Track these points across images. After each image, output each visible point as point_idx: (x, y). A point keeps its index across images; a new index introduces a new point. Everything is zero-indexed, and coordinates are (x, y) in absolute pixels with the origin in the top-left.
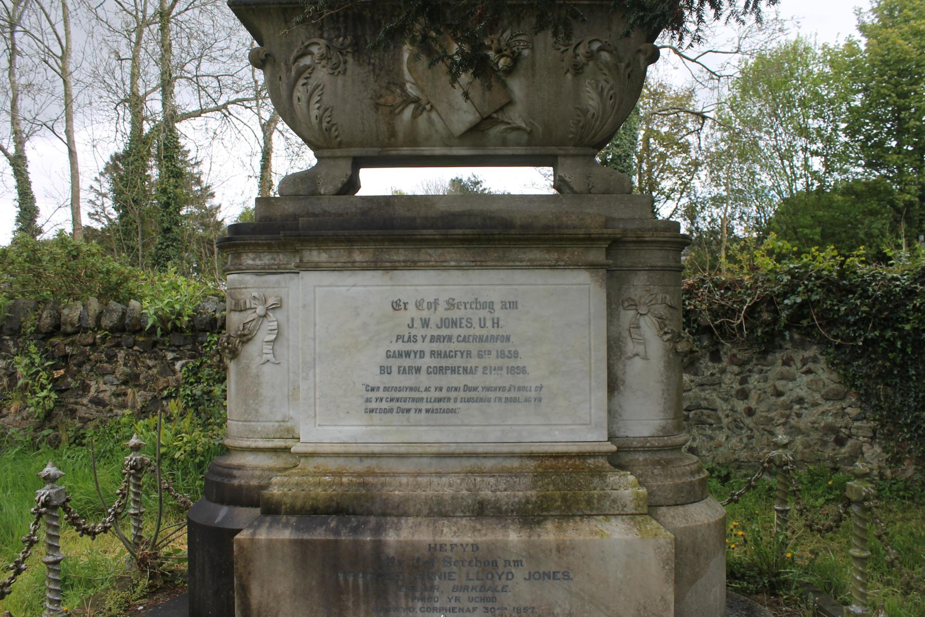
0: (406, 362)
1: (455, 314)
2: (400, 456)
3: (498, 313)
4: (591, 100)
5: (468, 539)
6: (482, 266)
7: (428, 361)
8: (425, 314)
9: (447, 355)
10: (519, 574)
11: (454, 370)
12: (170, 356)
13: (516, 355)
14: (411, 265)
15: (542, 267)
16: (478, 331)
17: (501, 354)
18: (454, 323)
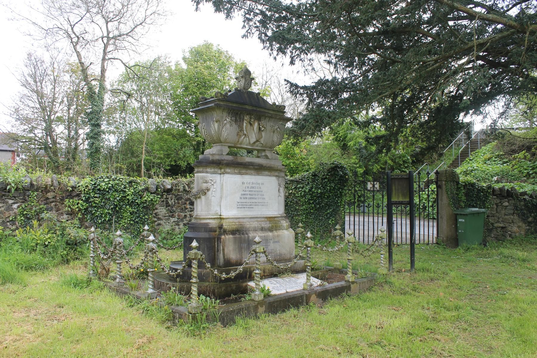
0: (245, 196)
1: (253, 185)
2: (244, 218)
3: (261, 186)
4: (275, 139)
5: (263, 235)
6: (258, 174)
7: (248, 196)
8: (248, 185)
9: (252, 195)
10: (272, 242)
11: (253, 198)
12: (11, 202)
13: (263, 195)
14: (247, 174)
15: (267, 176)
16: (257, 190)
17: (261, 195)
18: (253, 188)
